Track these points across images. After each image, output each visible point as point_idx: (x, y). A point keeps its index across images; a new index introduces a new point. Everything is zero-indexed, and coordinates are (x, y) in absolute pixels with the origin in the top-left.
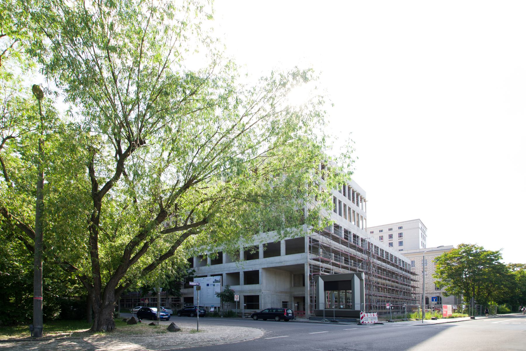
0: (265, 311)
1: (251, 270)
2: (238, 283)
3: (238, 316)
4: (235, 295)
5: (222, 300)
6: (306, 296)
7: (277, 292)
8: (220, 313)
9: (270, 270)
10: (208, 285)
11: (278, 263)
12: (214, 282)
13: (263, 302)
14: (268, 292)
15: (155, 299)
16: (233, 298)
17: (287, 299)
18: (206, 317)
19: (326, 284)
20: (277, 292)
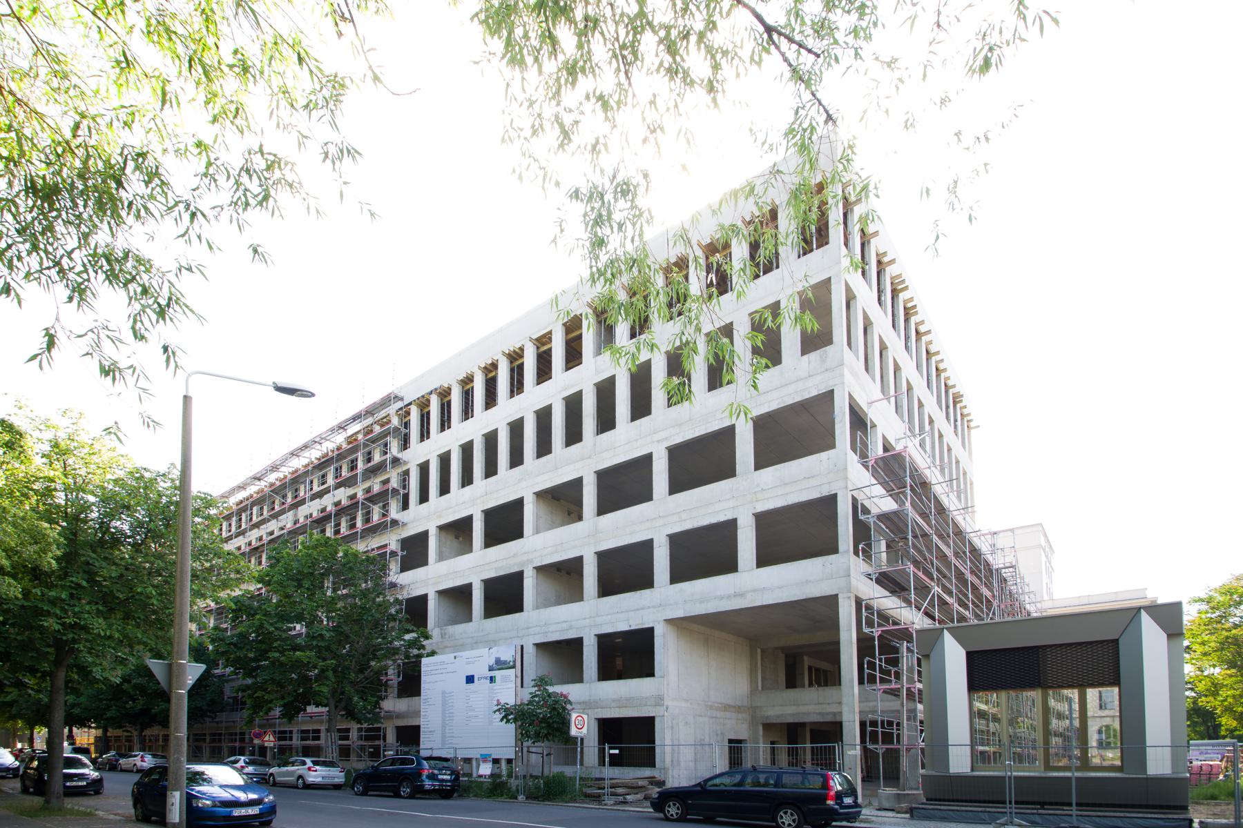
0: (717, 781)
1: (623, 627)
2: (577, 677)
3: (587, 796)
4: (574, 715)
5: (523, 735)
6: (846, 718)
7: (711, 708)
8: (513, 783)
9: (685, 625)
10: (470, 679)
11: (729, 597)
12: (491, 669)
13: (668, 742)
14: (683, 704)
15: (285, 732)
16: (565, 724)
17: (742, 732)
18: (461, 796)
19: (973, 658)
20: (711, 708)
